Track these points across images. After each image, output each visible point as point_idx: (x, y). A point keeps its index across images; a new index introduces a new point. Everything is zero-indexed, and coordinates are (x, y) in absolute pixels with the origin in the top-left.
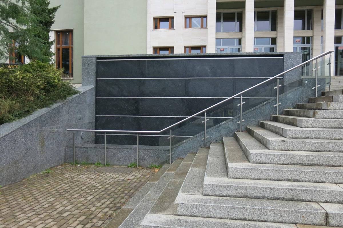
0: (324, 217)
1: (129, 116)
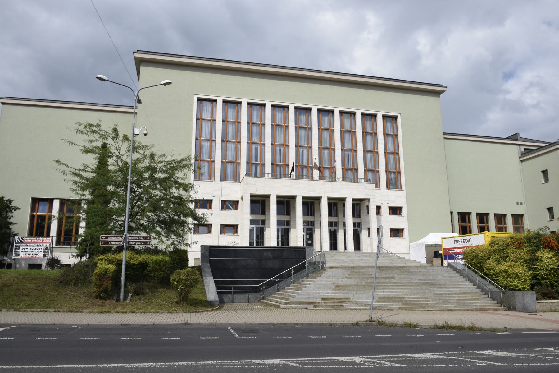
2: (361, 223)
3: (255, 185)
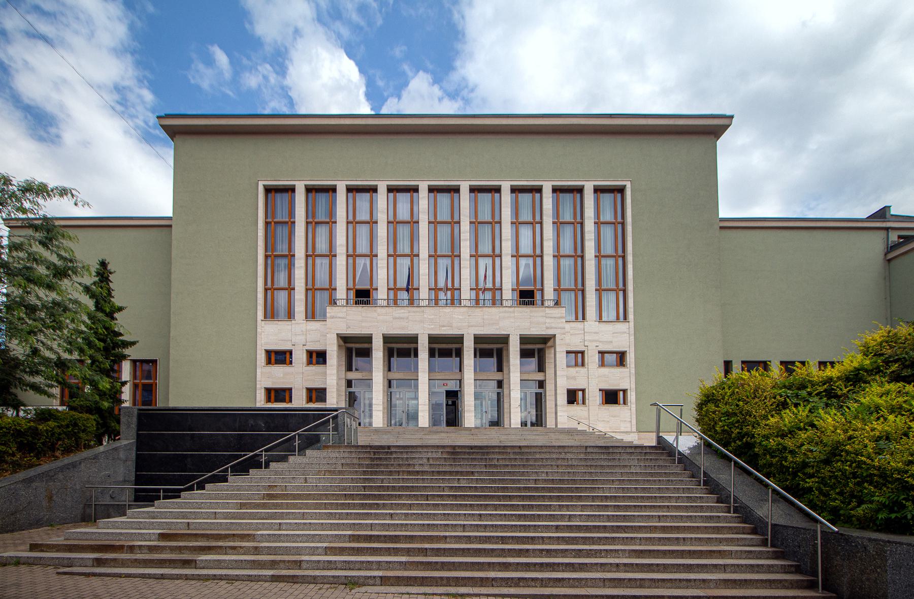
1: (486, 494)
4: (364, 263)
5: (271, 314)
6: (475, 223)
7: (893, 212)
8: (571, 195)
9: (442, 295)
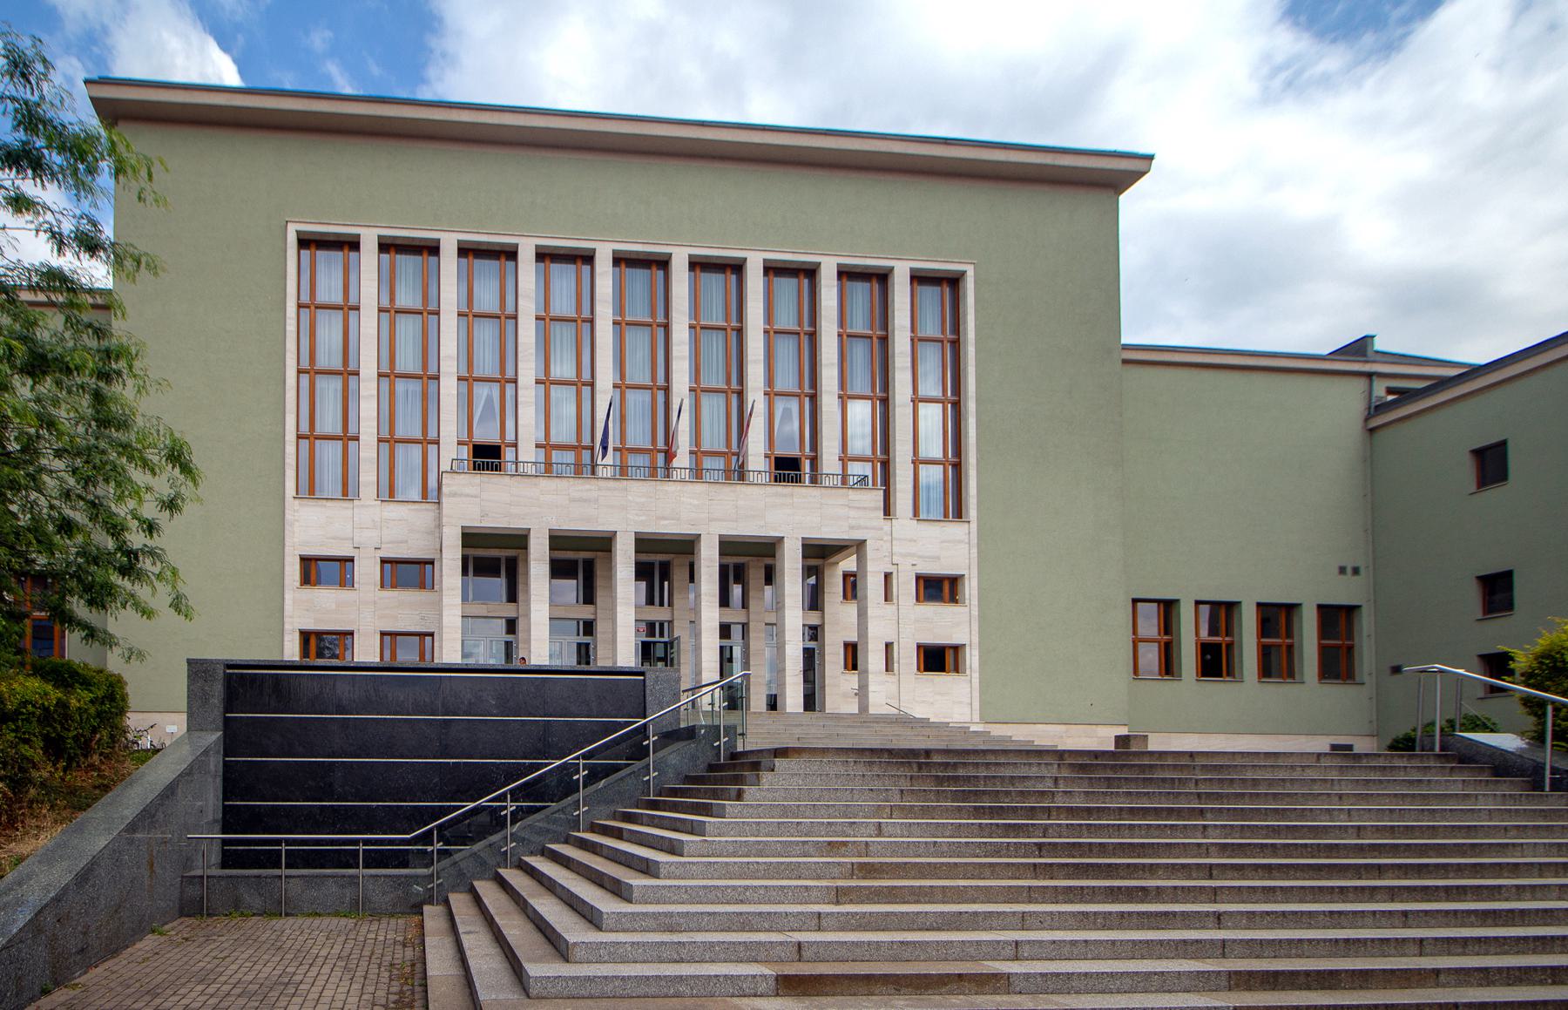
0: (796, 948)
2: (822, 626)
3: (476, 497)
4: (488, 395)
5: (310, 489)
6: (576, 321)
7: (1379, 345)
8: (647, 272)
9: (708, 463)
